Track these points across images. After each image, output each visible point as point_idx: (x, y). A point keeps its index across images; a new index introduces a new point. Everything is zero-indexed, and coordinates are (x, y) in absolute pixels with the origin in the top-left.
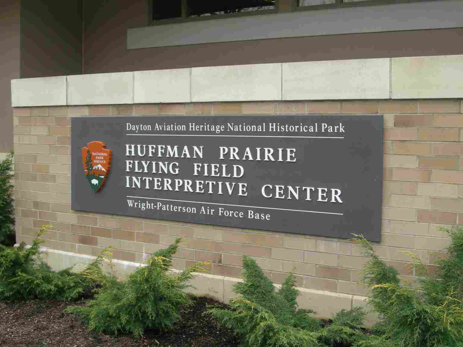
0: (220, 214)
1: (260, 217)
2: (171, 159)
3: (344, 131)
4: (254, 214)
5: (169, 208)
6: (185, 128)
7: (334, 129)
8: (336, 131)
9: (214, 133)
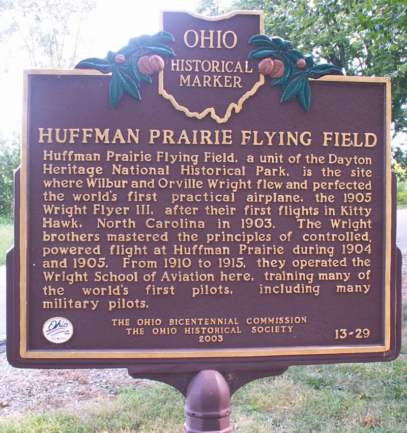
6: (370, 162)
7: (354, 288)
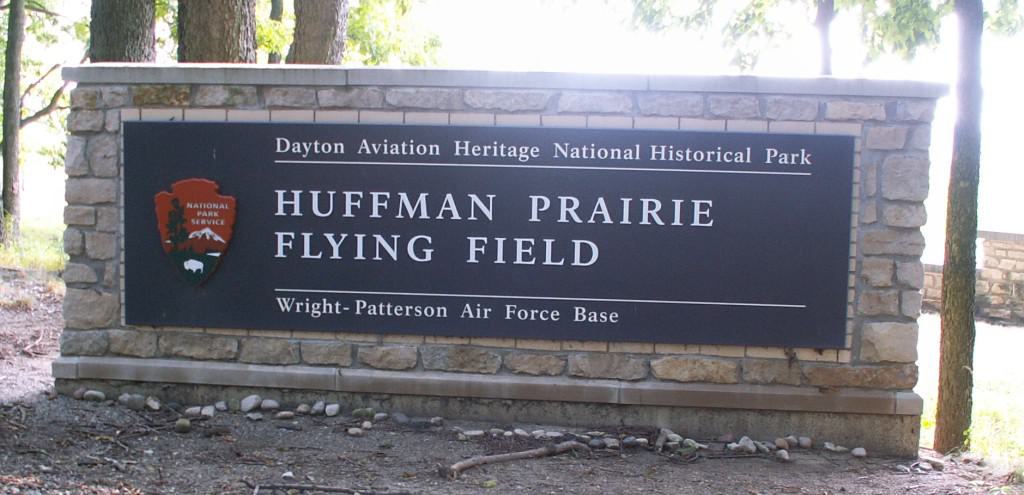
0: (508, 317)
1: (598, 317)
2: (411, 226)
3: (808, 163)
4: (586, 314)
5: (385, 310)
8: (793, 162)
9: (515, 160)
